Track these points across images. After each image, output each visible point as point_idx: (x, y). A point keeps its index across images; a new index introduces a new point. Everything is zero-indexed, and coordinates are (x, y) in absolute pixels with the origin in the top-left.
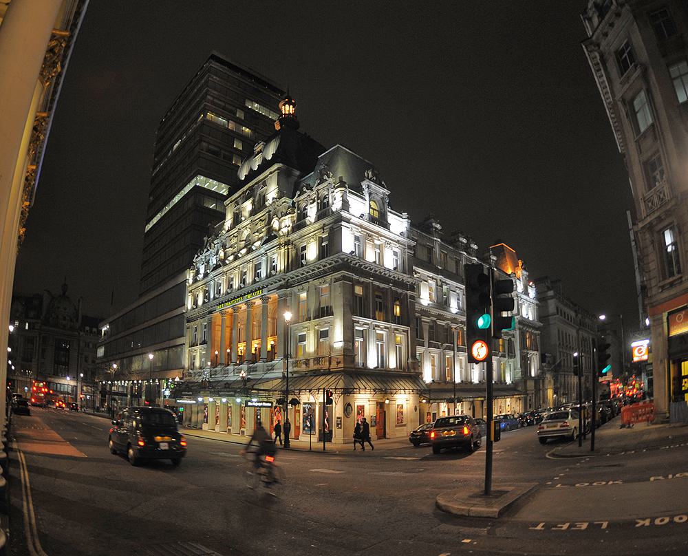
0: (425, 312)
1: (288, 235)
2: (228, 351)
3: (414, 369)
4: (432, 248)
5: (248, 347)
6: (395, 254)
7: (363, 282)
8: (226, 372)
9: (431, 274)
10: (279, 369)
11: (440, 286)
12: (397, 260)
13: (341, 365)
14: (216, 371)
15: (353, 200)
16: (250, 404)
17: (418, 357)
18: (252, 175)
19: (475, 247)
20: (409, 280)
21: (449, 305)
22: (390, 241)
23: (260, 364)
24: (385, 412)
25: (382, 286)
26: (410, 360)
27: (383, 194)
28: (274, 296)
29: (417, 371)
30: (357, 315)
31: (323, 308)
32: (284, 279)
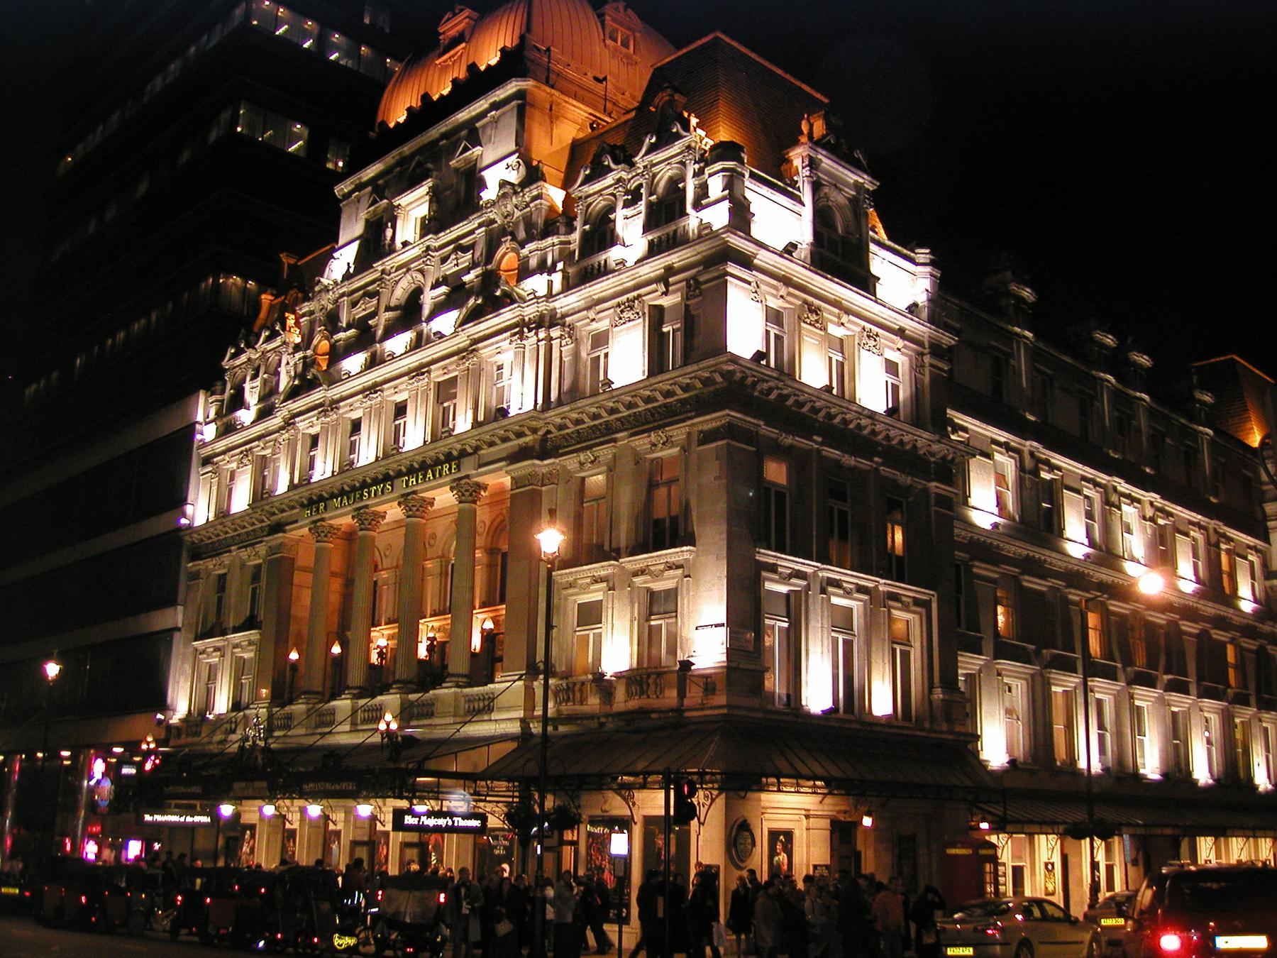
0: (982, 547)
1: (550, 295)
2: (336, 649)
3: (949, 720)
4: (1009, 355)
5: (408, 637)
6: (891, 367)
7: (791, 447)
8: (327, 720)
9: (1002, 436)
10: (509, 708)
11: (1028, 472)
12: (895, 389)
13: (721, 699)
14: (289, 717)
15: (761, 200)
16: (409, 820)
17: (962, 686)
18: (429, 112)
19: (1144, 360)
20: (935, 447)
21: (1061, 530)
22: (875, 329)
23: (445, 692)
24: (859, 853)
25: (850, 461)
26: (938, 695)
27: (857, 186)
28: (500, 479)
29: (958, 728)
30: (769, 548)
31: (658, 523)
32: (534, 431)
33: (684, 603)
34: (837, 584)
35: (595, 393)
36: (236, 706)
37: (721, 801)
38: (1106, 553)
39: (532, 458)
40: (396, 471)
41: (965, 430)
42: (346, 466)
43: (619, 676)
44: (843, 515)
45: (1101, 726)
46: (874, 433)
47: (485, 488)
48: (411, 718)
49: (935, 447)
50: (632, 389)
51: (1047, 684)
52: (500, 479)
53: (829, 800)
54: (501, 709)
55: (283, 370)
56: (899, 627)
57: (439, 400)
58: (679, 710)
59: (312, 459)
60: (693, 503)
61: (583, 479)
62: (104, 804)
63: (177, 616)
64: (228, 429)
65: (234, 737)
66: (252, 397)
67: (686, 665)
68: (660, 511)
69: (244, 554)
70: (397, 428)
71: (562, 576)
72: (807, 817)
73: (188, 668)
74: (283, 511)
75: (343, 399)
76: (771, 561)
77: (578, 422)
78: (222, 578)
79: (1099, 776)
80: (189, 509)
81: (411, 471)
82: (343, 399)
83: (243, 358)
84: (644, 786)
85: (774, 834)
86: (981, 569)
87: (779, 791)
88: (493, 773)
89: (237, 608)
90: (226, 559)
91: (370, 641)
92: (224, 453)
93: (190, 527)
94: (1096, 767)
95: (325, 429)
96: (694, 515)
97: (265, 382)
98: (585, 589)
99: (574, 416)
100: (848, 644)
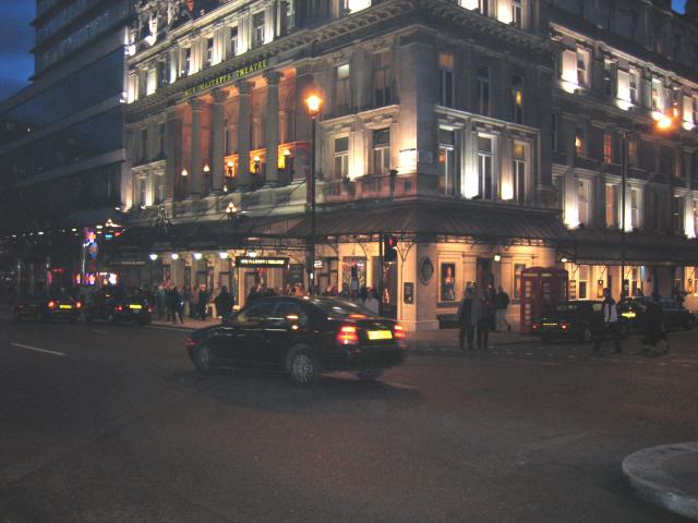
0: (569, 101)
2: (207, 169)
8: (204, 208)
9: (582, 38)
11: (597, 59)
12: (518, 10)
14: (184, 206)
20: (542, 45)
21: (616, 93)
23: (264, 190)
25: (490, 53)
31: (379, 92)
32: (308, 40)
33: (393, 138)
34: (482, 125)
35: (341, 17)
36: (157, 201)
37: (414, 248)
38: (643, 106)
39: (307, 56)
40: (232, 65)
41: (560, 35)
42: (206, 65)
43: (358, 179)
44: (486, 86)
45: (634, 206)
46: (505, 36)
47: (282, 75)
48: (247, 206)
49: (542, 45)
50: (362, 14)
51: (604, 182)
52: (290, 70)
53: (476, 247)
54: (295, 199)
55: (169, 12)
56: (519, 149)
57: (255, 25)
58: (389, 198)
59: (188, 63)
60: (398, 79)
61: (336, 68)
62: (94, 256)
63: (123, 154)
64: (142, 47)
65: (155, 219)
66: (153, 28)
67: (394, 173)
68: (380, 86)
69: (155, 118)
70: (233, 42)
71: (327, 123)
72: (464, 256)
73: (130, 182)
74: (173, 93)
75: (202, 27)
76: (444, 112)
77: (332, 34)
78: (145, 132)
79: (629, 233)
80: (124, 94)
81: (241, 67)
82: (202, 27)
83: (147, 6)
84: (371, 241)
85: (445, 266)
86: (567, 116)
87: (446, 242)
88: (291, 234)
89: (154, 145)
90: (146, 121)
91: (249, 159)
92: (140, 62)
93: (125, 104)
94: (628, 227)
95: (193, 46)
96: (399, 85)
97: (160, 20)
98: (338, 131)
99: (330, 30)
100: (488, 160)
